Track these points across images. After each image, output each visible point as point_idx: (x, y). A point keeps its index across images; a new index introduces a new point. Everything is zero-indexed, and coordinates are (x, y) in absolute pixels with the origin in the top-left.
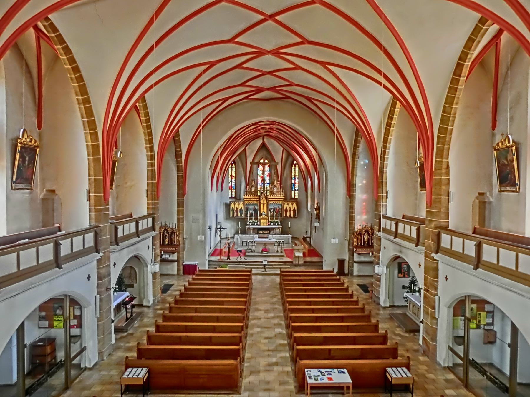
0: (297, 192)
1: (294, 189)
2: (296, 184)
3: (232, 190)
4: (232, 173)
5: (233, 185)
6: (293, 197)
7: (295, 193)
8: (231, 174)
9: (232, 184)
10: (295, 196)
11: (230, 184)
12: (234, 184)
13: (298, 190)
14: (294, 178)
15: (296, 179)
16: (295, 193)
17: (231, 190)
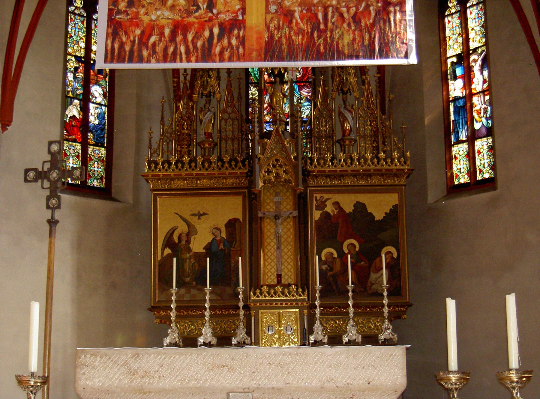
0: (482, 145)
1: (463, 136)
2: (475, 100)
3: (85, 145)
4: (88, 49)
5: (93, 120)
6: (463, 179)
7: (471, 156)
8: (82, 53)
9: (85, 110)
10: (472, 171)
11: (74, 111)
12: (100, 116)
13: (489, 132)
14: (459, 71)
15: (476, 68)
16: (471, 156)
17: (78, 146)
